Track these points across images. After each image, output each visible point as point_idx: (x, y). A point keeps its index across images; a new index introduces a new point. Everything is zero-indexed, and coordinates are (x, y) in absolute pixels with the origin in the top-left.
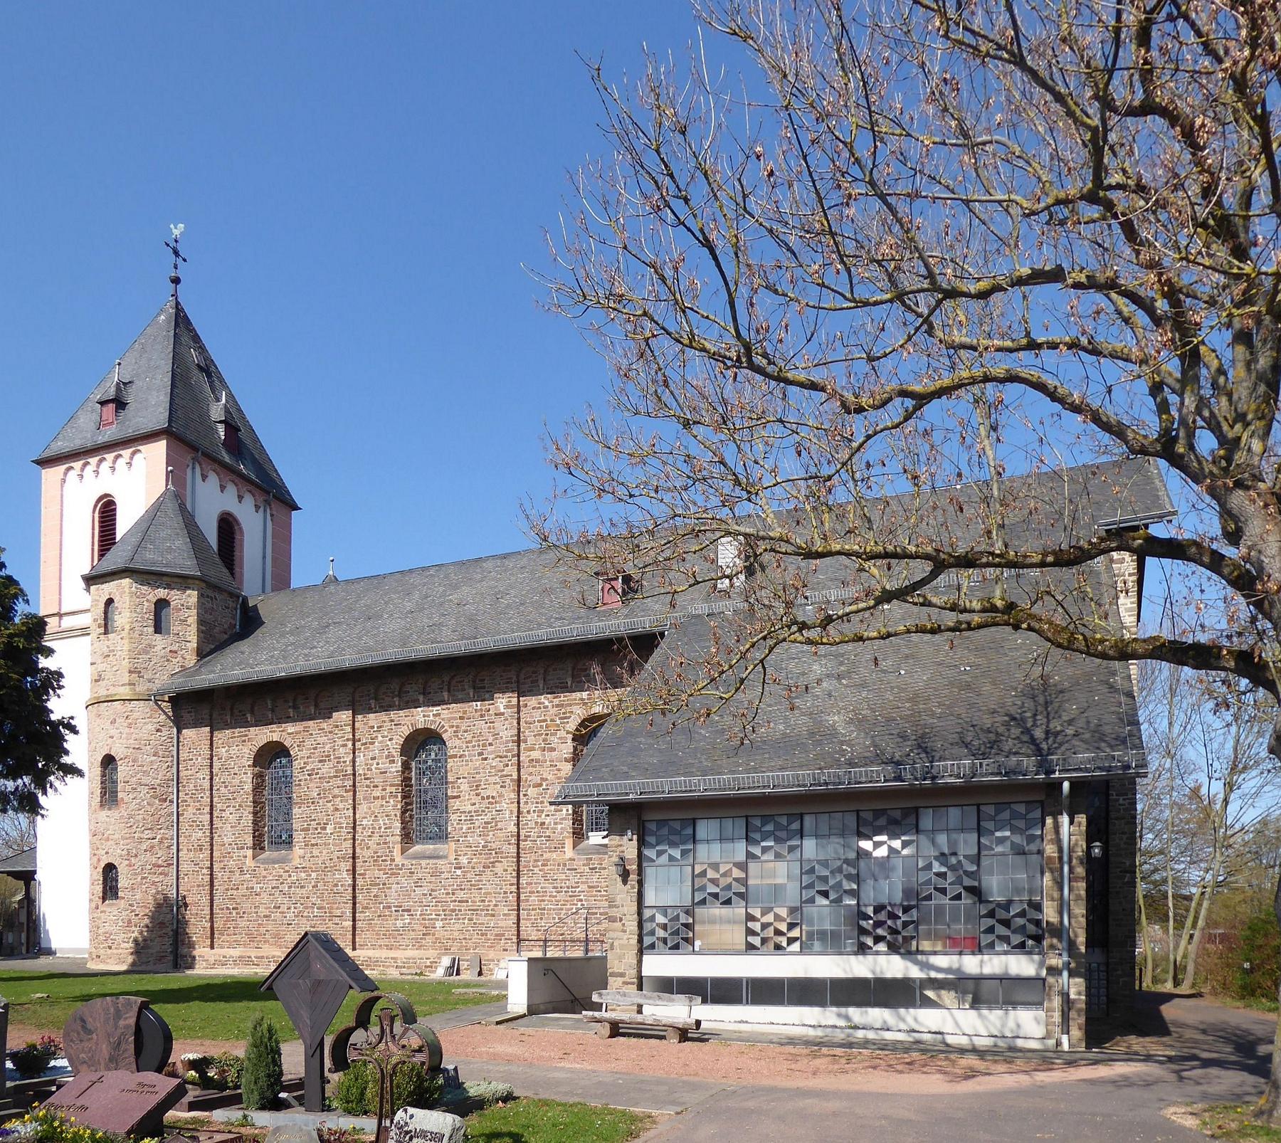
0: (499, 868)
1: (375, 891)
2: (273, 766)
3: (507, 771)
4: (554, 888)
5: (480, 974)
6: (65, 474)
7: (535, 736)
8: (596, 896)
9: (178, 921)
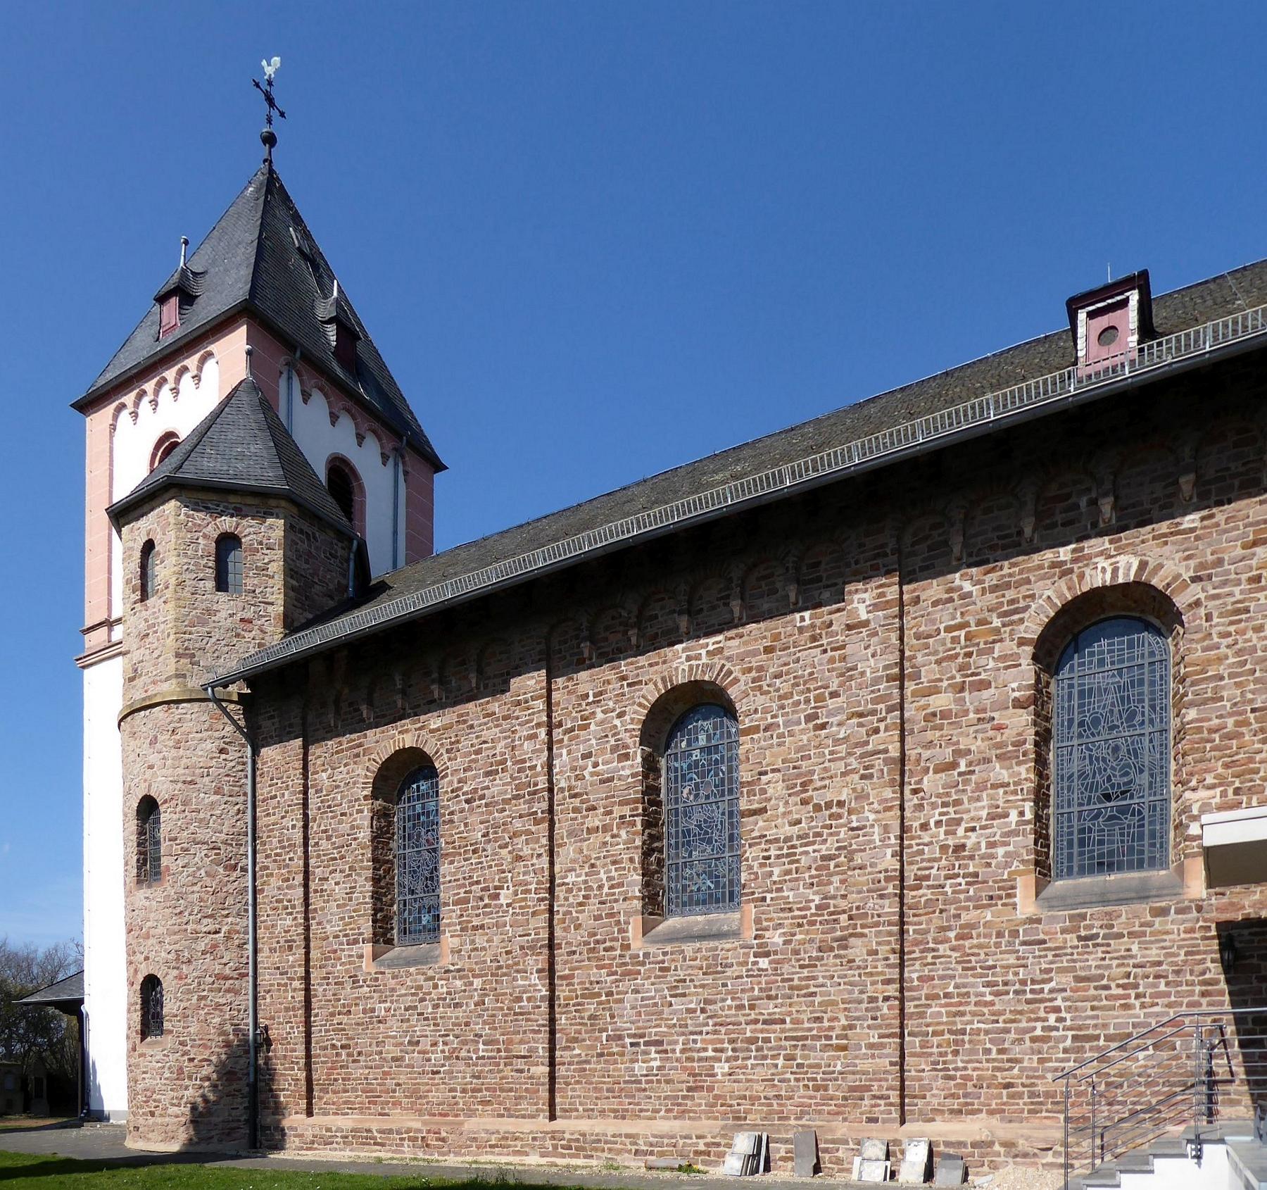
0: (858, 949)
1: (591, 1007)
2: (405, 797)
3: (874, 742)
4: (988, 984)
5: (817, 1169)
6: (115, 417)
7: (938, 662)
8: (1095, 998)
9: (257, 1067)
